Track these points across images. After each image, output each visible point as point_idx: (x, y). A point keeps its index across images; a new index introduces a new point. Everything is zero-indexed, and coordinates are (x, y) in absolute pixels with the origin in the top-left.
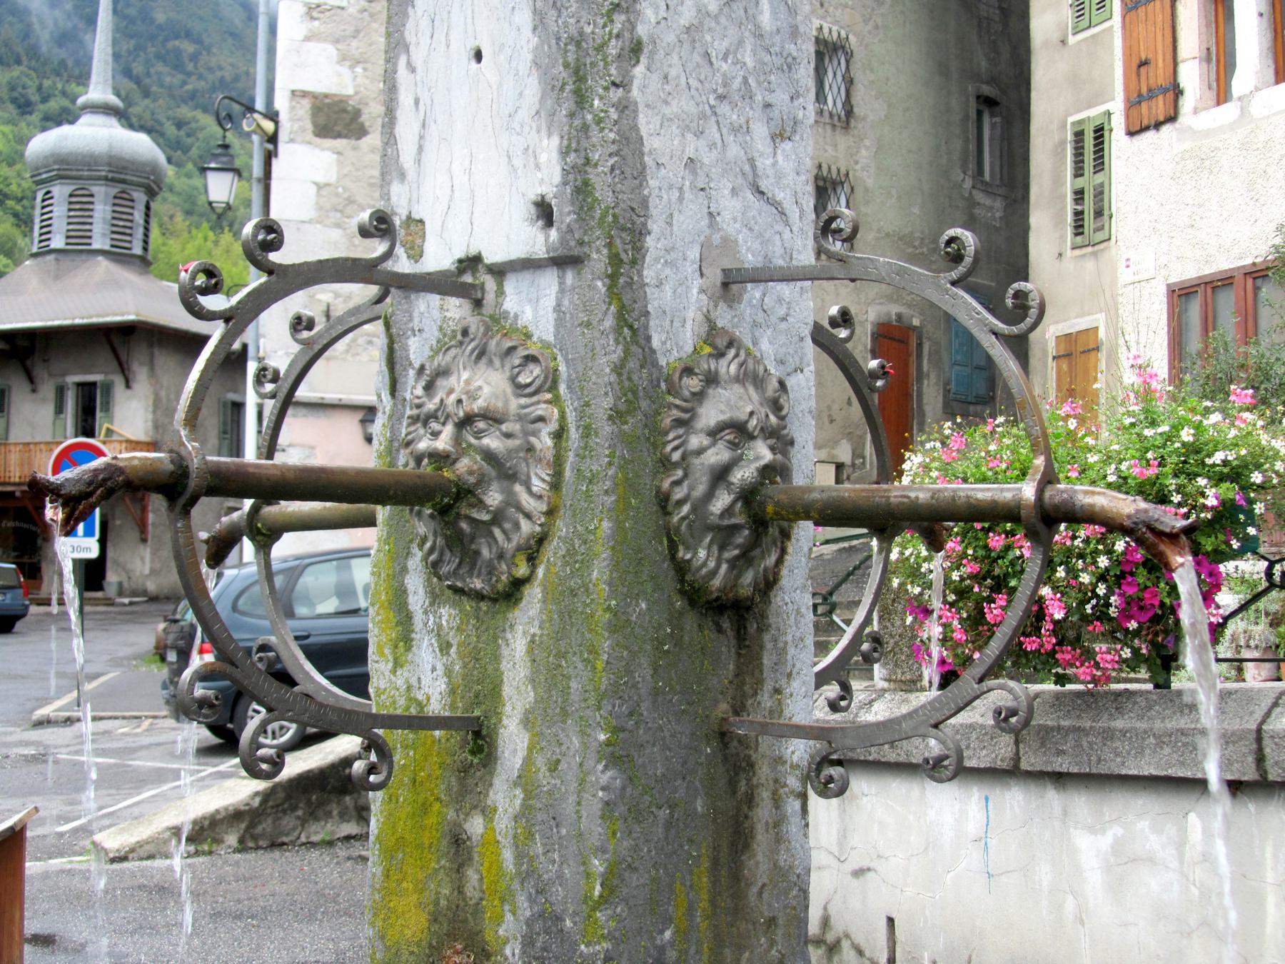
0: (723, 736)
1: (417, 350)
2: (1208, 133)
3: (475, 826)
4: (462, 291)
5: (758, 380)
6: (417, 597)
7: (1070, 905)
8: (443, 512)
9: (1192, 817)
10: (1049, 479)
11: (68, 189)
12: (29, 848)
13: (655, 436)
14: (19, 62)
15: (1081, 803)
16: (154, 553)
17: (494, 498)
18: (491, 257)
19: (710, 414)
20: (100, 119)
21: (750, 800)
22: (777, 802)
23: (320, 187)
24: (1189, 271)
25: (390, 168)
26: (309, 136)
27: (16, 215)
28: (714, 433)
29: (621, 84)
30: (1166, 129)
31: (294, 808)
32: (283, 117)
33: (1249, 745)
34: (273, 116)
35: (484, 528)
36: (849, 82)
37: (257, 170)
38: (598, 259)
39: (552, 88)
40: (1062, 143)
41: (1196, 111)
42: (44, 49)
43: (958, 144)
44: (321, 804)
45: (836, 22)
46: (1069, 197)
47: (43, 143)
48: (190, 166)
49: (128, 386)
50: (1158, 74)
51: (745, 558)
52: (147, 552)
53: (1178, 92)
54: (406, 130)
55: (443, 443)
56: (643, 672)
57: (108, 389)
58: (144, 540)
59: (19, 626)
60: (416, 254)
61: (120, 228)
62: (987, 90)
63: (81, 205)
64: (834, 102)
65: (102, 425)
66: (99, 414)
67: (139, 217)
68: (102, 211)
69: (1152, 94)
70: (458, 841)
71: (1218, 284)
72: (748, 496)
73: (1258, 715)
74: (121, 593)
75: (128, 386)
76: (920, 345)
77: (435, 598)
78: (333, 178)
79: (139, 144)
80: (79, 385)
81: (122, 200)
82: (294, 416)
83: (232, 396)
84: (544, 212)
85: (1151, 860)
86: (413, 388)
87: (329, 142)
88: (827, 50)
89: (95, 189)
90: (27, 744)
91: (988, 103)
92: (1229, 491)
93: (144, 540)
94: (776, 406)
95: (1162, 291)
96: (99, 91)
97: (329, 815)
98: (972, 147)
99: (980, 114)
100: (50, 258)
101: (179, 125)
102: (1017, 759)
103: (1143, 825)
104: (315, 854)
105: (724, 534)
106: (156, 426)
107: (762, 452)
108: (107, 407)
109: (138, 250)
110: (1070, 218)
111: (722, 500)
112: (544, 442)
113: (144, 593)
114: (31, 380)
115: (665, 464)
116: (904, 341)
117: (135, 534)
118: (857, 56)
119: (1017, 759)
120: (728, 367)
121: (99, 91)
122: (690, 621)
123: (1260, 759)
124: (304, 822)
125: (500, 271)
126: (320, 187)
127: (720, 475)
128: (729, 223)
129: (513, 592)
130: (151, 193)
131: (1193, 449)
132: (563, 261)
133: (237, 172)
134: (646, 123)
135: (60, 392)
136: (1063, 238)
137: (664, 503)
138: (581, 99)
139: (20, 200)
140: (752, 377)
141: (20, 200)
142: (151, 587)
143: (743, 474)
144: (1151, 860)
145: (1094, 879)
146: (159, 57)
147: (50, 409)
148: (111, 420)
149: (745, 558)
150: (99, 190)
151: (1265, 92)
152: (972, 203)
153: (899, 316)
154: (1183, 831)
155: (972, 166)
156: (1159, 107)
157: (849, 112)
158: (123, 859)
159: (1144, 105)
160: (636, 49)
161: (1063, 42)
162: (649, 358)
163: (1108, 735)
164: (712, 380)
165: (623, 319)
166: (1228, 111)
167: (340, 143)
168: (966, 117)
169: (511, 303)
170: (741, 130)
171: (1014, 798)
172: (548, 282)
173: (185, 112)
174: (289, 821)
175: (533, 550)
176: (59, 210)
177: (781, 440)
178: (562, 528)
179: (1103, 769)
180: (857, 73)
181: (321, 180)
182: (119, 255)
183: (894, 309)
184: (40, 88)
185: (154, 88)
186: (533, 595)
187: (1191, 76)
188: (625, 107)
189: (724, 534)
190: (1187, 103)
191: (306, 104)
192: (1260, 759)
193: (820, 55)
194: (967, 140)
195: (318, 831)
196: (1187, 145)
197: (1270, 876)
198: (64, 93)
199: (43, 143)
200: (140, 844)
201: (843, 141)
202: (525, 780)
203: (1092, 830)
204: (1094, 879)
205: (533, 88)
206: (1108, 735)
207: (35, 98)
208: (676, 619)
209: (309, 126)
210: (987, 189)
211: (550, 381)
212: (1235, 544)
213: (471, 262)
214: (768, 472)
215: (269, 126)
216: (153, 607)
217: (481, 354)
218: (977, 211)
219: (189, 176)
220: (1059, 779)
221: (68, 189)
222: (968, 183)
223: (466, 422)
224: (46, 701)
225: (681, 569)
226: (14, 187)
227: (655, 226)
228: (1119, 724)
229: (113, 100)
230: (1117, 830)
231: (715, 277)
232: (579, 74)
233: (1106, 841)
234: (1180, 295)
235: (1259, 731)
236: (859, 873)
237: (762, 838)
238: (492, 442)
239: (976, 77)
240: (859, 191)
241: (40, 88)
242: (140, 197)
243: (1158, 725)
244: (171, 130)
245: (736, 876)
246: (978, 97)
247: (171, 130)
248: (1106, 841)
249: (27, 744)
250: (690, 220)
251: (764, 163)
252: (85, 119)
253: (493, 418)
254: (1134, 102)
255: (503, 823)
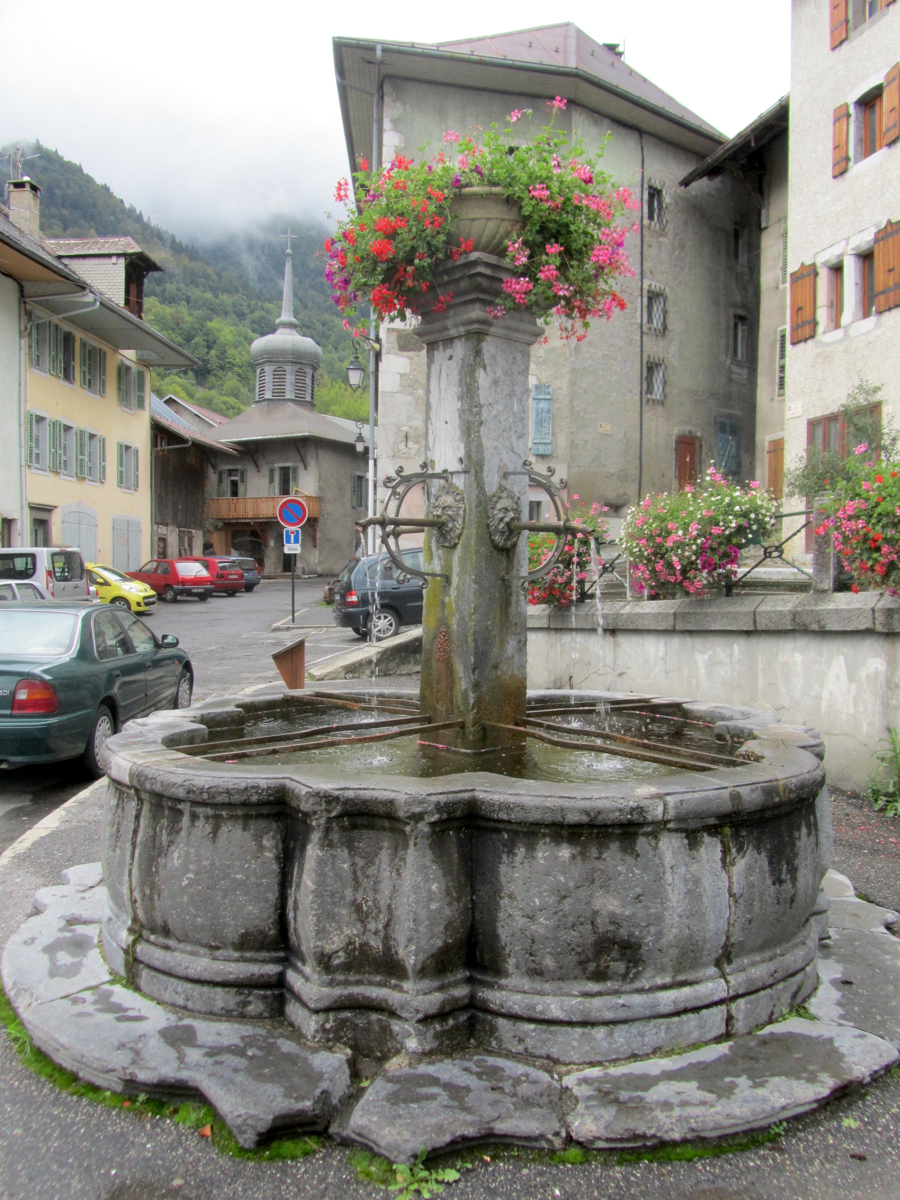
0: (503, 580)
1: (434, 491)
2: (829, 344)
3: (447, 599)
4: (443, 478)
5: (512, 498)
6: (434, 549)
7: (694, 682)
8: (440, 528)
9: (735, 646)
10: (567, 520)
11: (272, 368)
12: (306, 650)
13: (486, 511)
14: (237, 291)
15: (698, 642)
16: (320, 553)
17: (450, 525)
18: (450, 470)
19: (499, 506)
20: (287, 331)
21: (510, 595)
22: (518, 596)
23: (402, 375)
24: (818, 412)
25: (427, 448)
26: (396, 350)
27: (239, 375)
28: (500, 510)
29: (478, 432)
30: (810, 342)
31: (394, 659)
32: (384, 341)
33: (751, 616)
34: (378, 340)
35: (448, 532)
36: (665, 312)
37: (371, 368)
38: (473, 471)
39: (462, 432)
40: (775, 341)
41: (824, 333)
42: (251, 283)
43: (723, 342)
44: (406, 658)
45: (659, 281)
46: (777, 369)
47: (260, 343)
48: (330, 346)
49: (306, 468)
50: (806, 314)
51: (508, 539)
52: (316, 552)
53: (815, 323)
54: (430, 439)
55: (439, 513)
56: (483, 564)
57: (295, 470)
58: (315, 546)
59: (255, 588)
60: (433, 469)
61: (299, 387)
62: (740, 312)
63: (279, 376)
64: (657, 323)
65: (293, 488)
66: (291, 483)
67: (308, 381)
68: (290, 379)
69: (803, 324)
70: (443, 603)
71: (831, 418)
72: (508, 524)
73: (756, 604)
74: (304, 573)
75: (306, 468)
76: (701, 446)
77: (438, 548)
78: (408, 371)
79: (308, 343)
80: (281, 468)
81: (300, 373)
82: (851, 1069)
83: (358, 473)
84: (461, 460)
85: (721, 663)
86: (433, 500)
87: (406, 354)
88: (653, 297)
89: (286, 368)
90: (271, 638)
91: (740, 319)
92: (742, 521)
93: (315, 546)
94: (517, 503)
95: (805, 422)
96: (286, 316)
97: (409, 662)
98: (731, 343)
99: (736, 325)
100: (265, 403)
101: (324, 324)
102: (674, 626)
103: (719, 649)
104: (403, 678)
105: (503, 533)
106: (320, 489)
107: (511, 515)
108: (295, 479)
109: (308, 399)
110: (777, 380)
111: (502, 525)
112: (461, 513)
113: (316, 573)
114: (257, 466)
115: (488, 517)
116: (692, 444)
117: (311, 544)
118: (669, 299)
119: (674, 626)
120: (504, 494)
121: (286, 316)
122: (495, 553)
123: (755, 622)
124: (399, 665)
125: (452, 473)
126: (402, 375)
127: (501, 520)
128: (505, 461)
129: (454, 546)
130: (315, 369)
131: (729, 505)
132: (466, 472)
133: (363, 370)
134: (484, 440)
135: (272, 472)
136: (774, 391)
137: (488, 526)
138: (469, 435)
139: (241, 367)
140: (511, 496)
141: (241, 367)
142: (319, 570)
143: (507, 520)
144: (721, 663)
145: (702, 672)
146: (312, 287)
147: (266, 481)
148: (297, 486)
149: (508, 539)
150: (288, 368)
151: (856, 324)
152: (730, 372)
153: (690, 432)
154: (732, 651)
155: (731, 353)
156: (807, 331)
157: (665, 328)
158: (322, 679)
159: (800, 330)
160: (481, 423)
161: (777, 288)
162: (484, 493)
163: (706, 615)
164: (500, 498)
165: (478, 485)
166: (839, 333)
167: (411, 354)
168: (728, 327)
169: (454, 481)
170: (509, 438)
171: (675, 642)
172: (462, 477)
173: (327, 317)
174: (392, 665)
175: (459, 537)
176: (269, 379)
177: (517, 511)
178: (465, 532)
179: (704, 628)
180: (669, 307)
181: (402, 372)
182: (299, 401)
183: (687, 428)
184: (249, 306)
185: (310, 304)
186: (459, 547)
187: (822, 315)
188: (479, 437)
189: (503, 533)
190: (820, 329)
191: (395, 335)
192: (755, 622)
193: (650, 299)
194: (728, 340)
195: (405, 669)
196: (820, 350)
197: (760, 667)
198: (262, 308)
199: (260, 343)
200: (329, 673)
201: (662, 343)
202: (458, 588)
203: (702, 652)
204: (702, 672)
205: (458, 432)
206: (706, 615)
207: (247, 311)
208: (491, 552)
209: (396, 346)
210: (739, 364)
211: (463, 499)
212: (744, 541)
213: (445, 471)
214: (513, 519)
215: (377, 346)
216: (320, 579)
217: (448, 492)
218: (733, 376)
219: (330, 352)
220: (690, 633)
221: (272, 368)
222: (729, 362)
223: (444, 508)
224: (276, 621)
225: (492, 541)
226: (238, 360)
227: (486, 463)
228: (710, 610)
229: (293, 320)
230: (710, 652)
231: (502, 473)
232: (468, 429)
233: (706, 657)
234: (812, 425)
235: (755, 613)
236: (620, 675)
237: (513, 604)
238: (450, 513)
239: (734, 305)
240: (669, 368)
241: (249, 306)
242: (309, 371)
243: (722, 610)
244: (319, 327)
245: (507, 612)
246: (735, 316)
247: (319, 327)
248: (706, 657)
249: (271, 638)
250: (495, 461)
251: (515, 445)
252: (279, 331)
253: (450, 507)
254: (794, 329)
255: (453, 598)
